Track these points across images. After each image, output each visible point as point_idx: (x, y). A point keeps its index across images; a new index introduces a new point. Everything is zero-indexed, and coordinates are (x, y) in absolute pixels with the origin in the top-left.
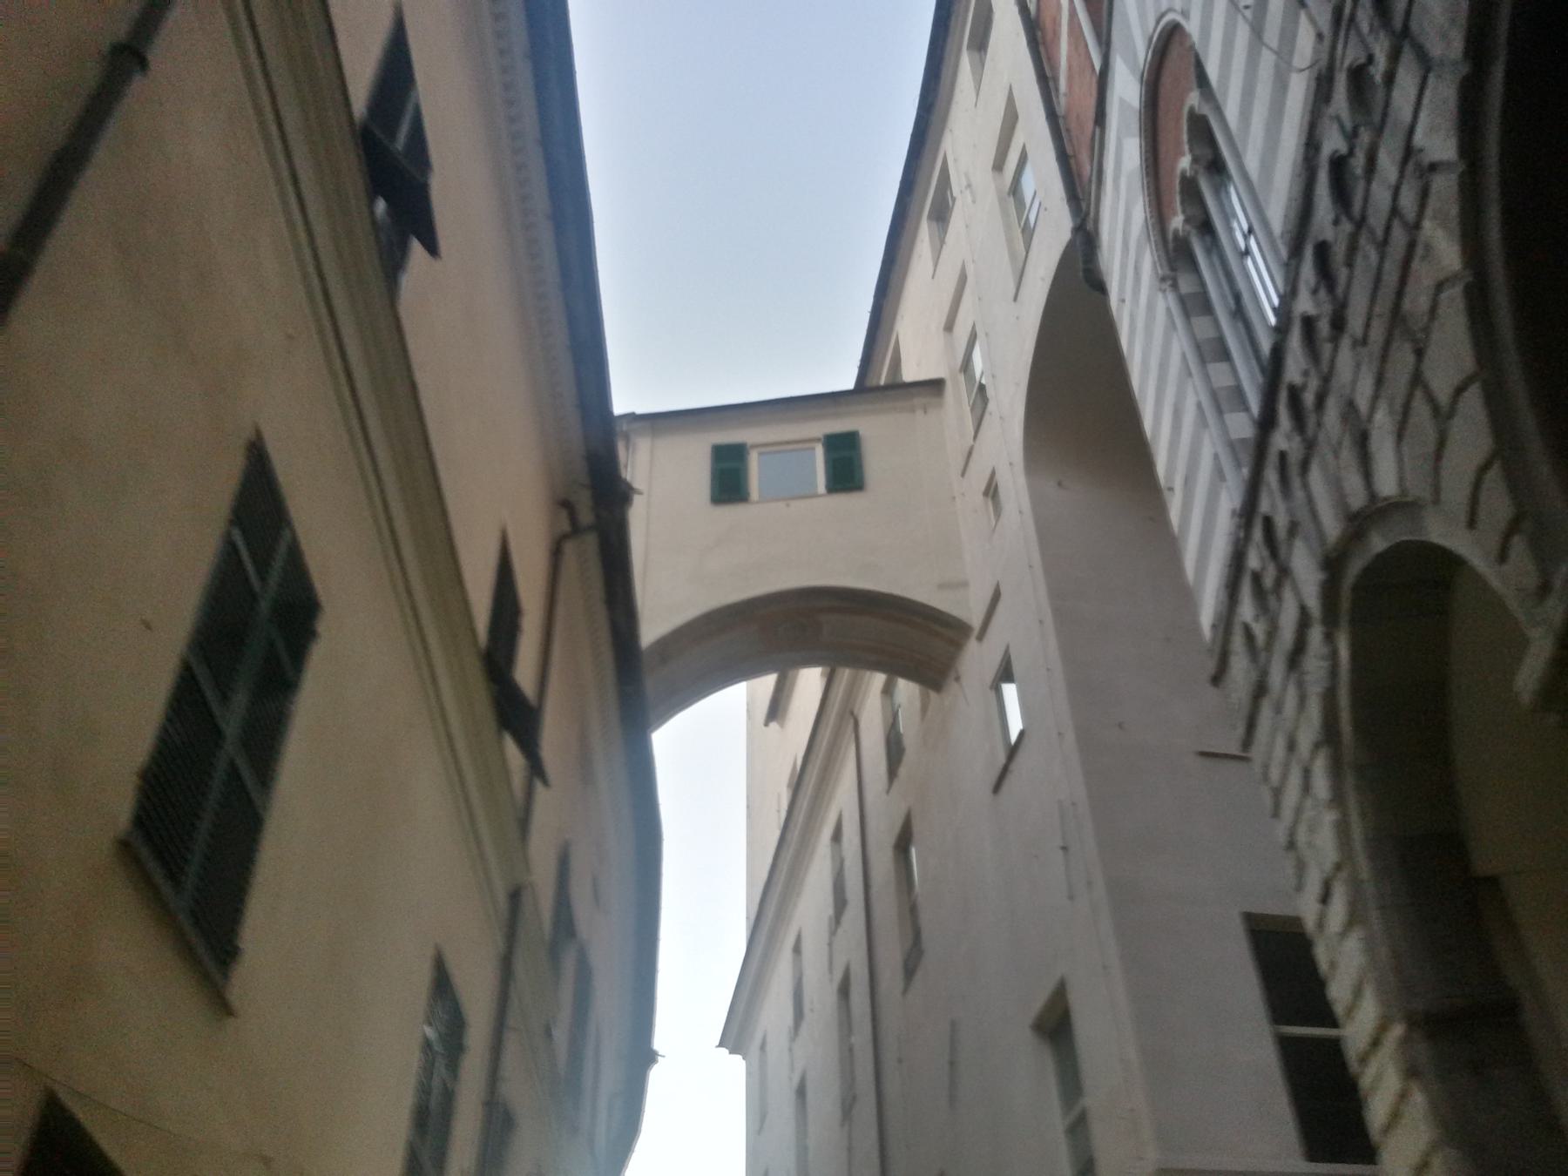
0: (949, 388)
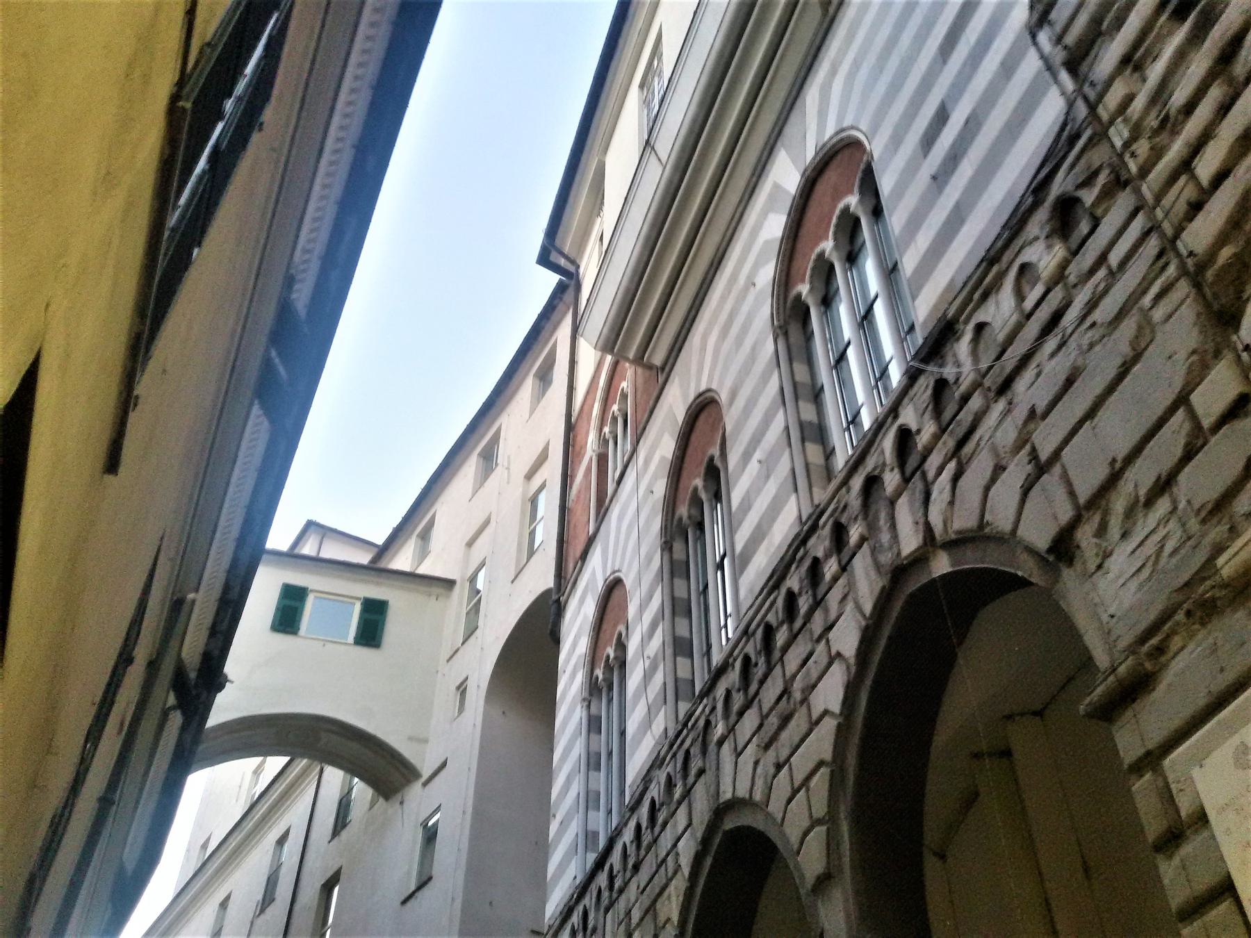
0: (457, 588)
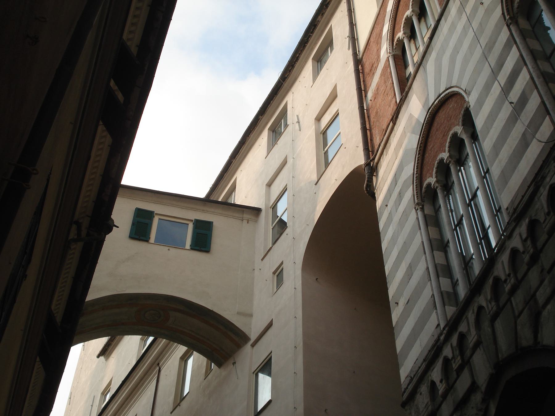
0: (263, 214)
